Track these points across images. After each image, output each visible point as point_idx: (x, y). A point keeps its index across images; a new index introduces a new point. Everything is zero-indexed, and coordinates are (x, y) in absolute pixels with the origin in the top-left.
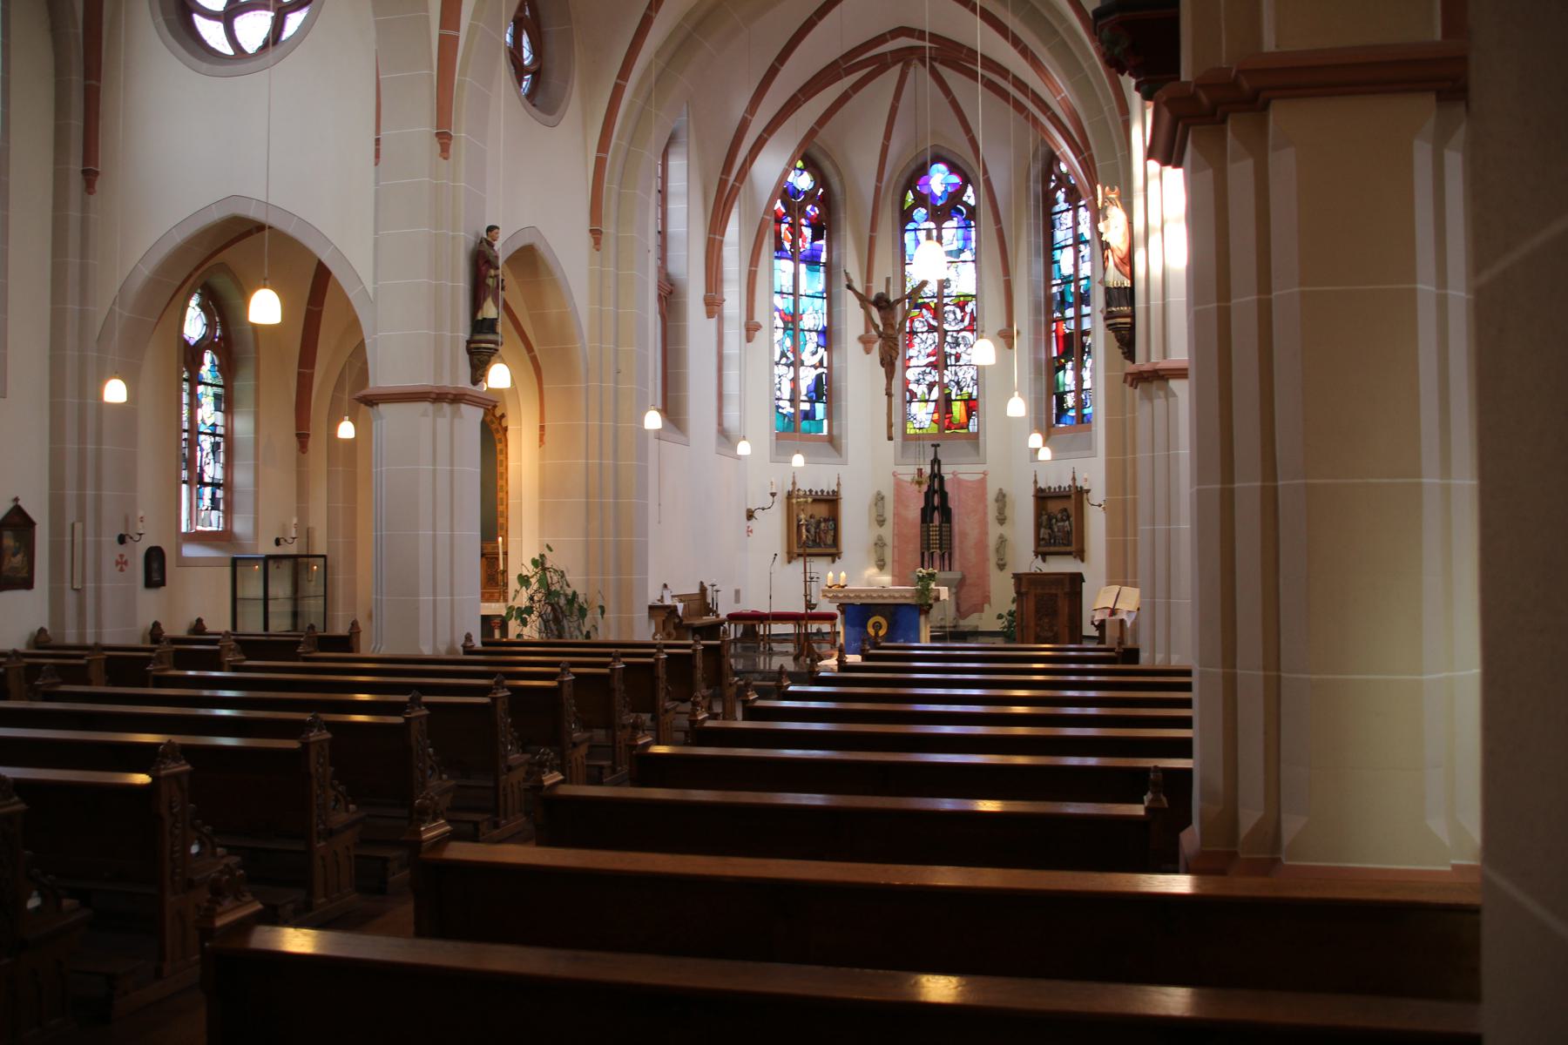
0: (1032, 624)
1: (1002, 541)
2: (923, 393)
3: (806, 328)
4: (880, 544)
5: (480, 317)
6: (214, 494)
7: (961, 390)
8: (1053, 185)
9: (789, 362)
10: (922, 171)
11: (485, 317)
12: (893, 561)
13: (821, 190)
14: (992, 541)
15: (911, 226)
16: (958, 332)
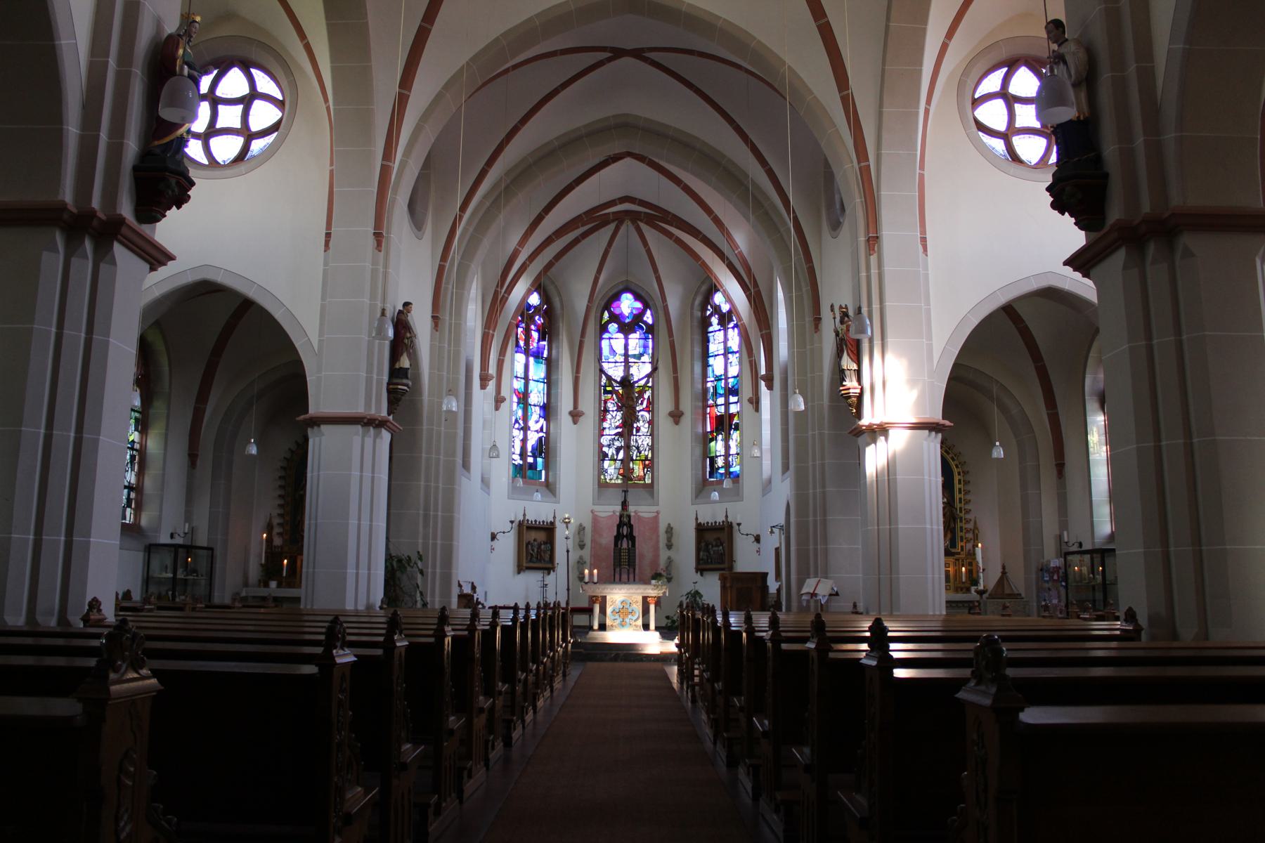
2: (613, 454)
3: (532, 404)
5: (397, 366)
6: (129, 495)
7: (640, 453)
8: (708, 313)
10: (616, 297)
11: (402, 366)
13: (545, 306)
15: (606, 336)
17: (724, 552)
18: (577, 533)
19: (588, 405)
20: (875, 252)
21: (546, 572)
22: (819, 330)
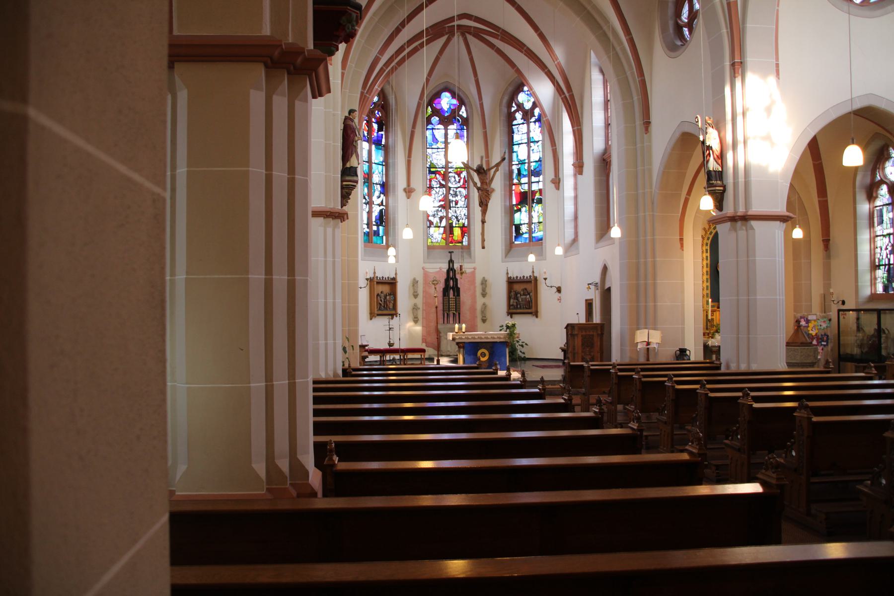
0: (580, 351)
1: (485, 306)
2: (437, 222)
3: (375, 183)
4: (415, 308)
5: (348, 165)
7: (458, 221)
8: (513, 109)
9: (367, 202)
10: (437, 95)
12: (423, 318)
14: (479, 307)
15: (430, 127)
16: (457, 188)
17: (531, 301)
18: (412, 285)
19: (418, 182)
20: (739, 75)
21: (390, 317)
22: (648, 132)
